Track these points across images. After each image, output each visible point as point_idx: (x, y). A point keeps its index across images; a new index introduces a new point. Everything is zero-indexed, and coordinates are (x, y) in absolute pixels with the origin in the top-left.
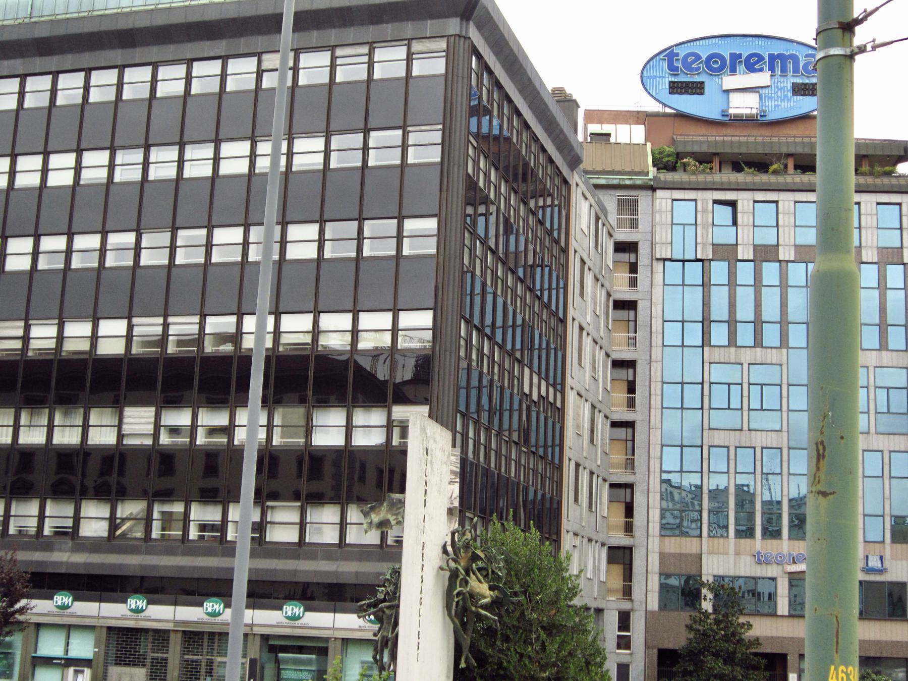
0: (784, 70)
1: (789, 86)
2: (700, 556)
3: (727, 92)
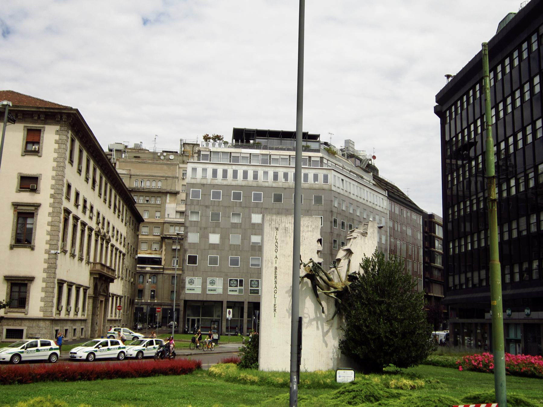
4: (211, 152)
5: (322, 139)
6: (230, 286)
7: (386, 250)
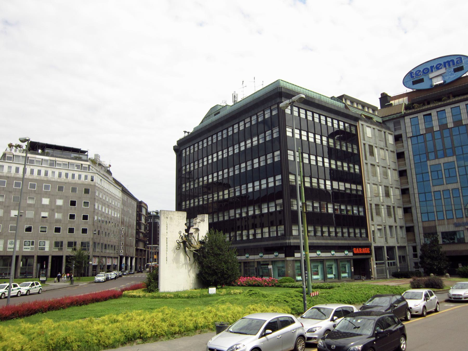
0: (449, 66)
1: (452, 70)
2: (435, 227)
3: (431, 79)
4: (14, 155)
5: (91, 155)
6: (25, 245)
7: (119, 222)
